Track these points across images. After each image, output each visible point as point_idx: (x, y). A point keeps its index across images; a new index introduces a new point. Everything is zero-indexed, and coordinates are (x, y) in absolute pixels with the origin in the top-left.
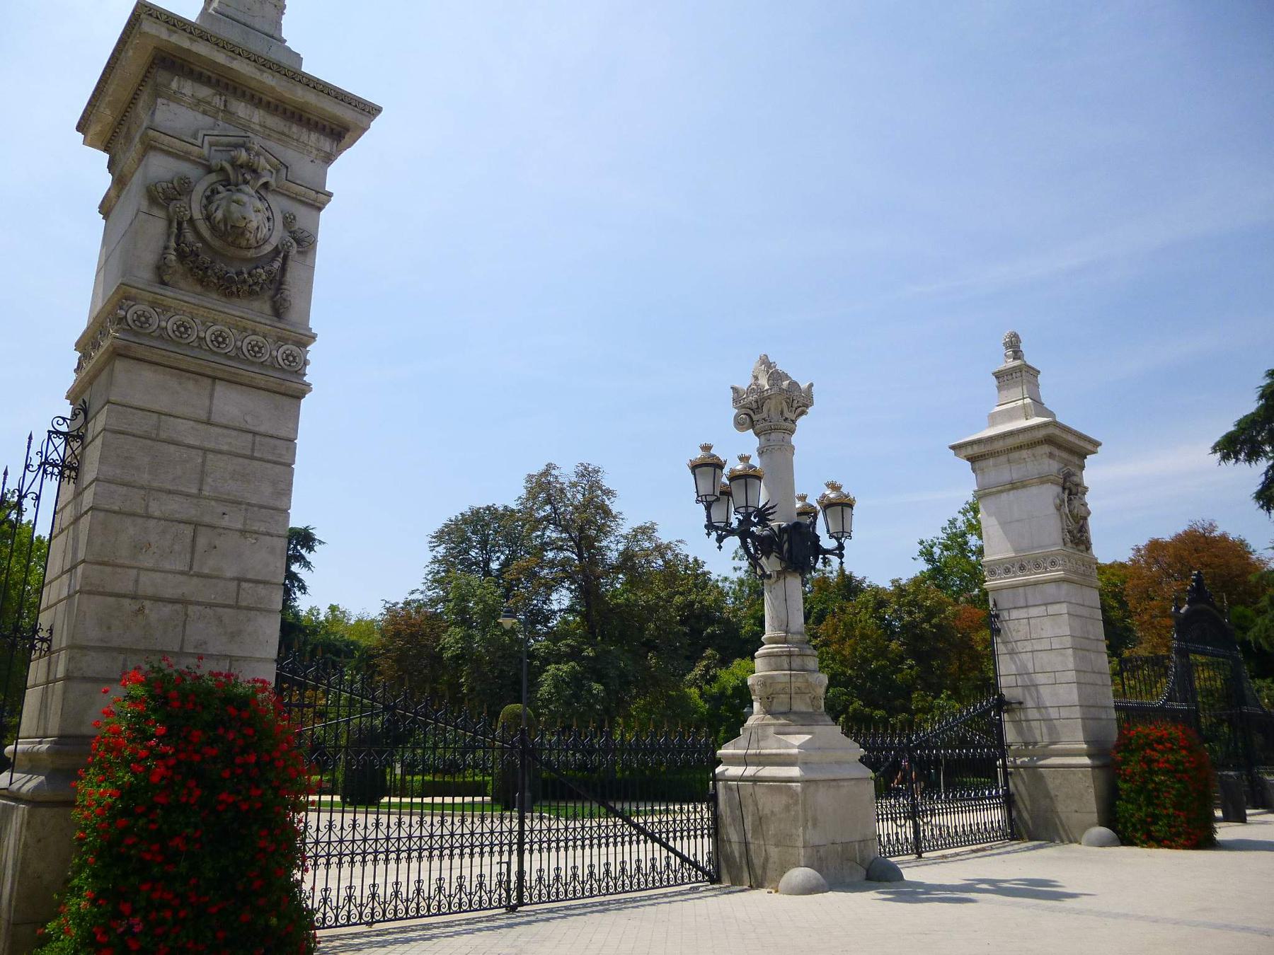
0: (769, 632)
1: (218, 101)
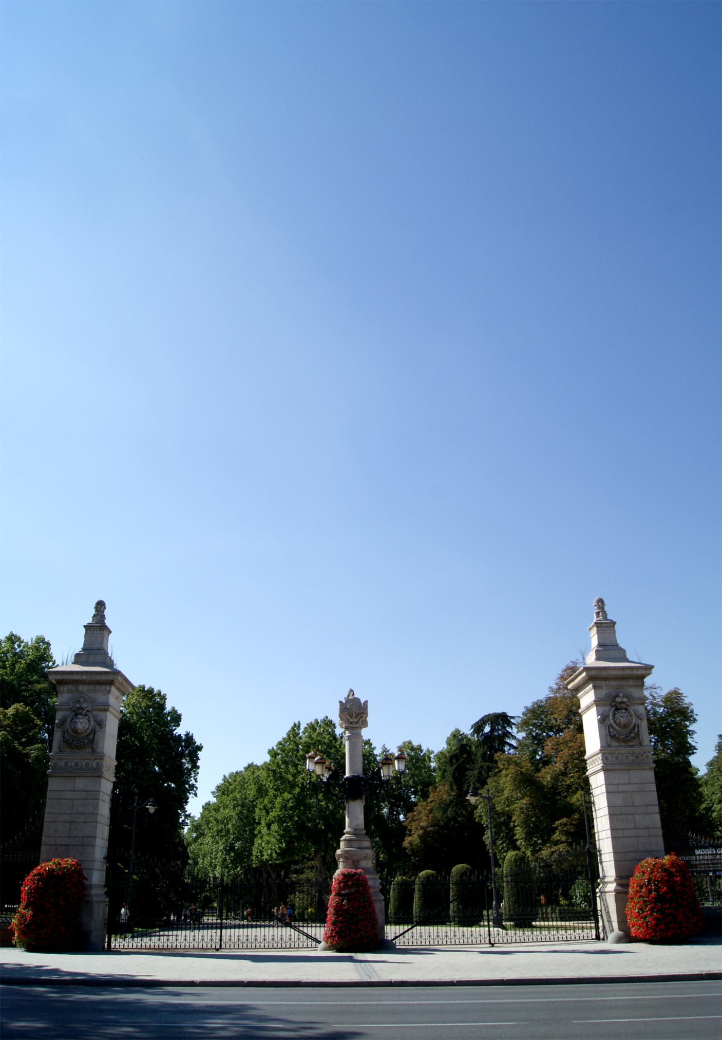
0: (347, 829)
1: (74, 688)
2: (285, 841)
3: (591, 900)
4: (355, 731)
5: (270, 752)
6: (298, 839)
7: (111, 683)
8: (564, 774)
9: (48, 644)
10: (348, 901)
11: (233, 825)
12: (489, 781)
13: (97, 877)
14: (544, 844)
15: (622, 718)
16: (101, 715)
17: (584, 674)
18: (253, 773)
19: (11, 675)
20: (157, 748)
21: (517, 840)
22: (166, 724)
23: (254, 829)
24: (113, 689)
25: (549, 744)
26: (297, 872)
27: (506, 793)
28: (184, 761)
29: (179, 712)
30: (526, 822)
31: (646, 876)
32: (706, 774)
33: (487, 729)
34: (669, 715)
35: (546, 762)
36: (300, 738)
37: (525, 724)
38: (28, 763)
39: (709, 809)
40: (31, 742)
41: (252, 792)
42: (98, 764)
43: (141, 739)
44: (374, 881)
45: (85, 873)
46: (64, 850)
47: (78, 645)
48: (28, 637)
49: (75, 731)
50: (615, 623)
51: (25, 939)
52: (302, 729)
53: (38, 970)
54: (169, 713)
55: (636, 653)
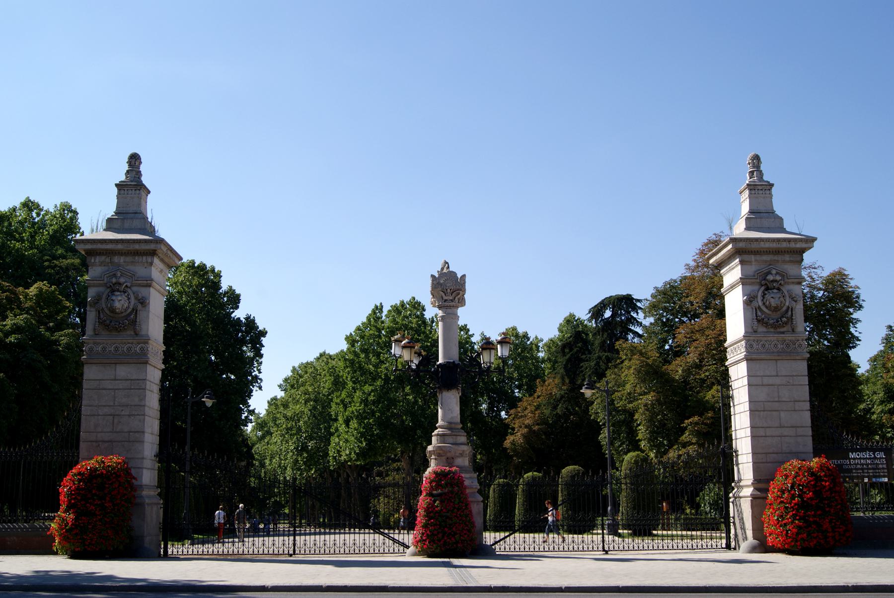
0: (440, 422)
1: (108, 260)
2: (365, 440)
3: (722, 506)
4: (449, 311)
5: (347, 338)
6: (381, 438)
7: (153, 253)
8: (699, 366)
9: (75, 213)
10: (441, 502)
11: (305, 423)
12: (608, 373)
13: (148, 476)
14: (671, 446)
15: (773, 299)
16: (143, 291)
17: (730, 246)
18: (327, 363)
19: (31, 248)
20: (212, 334)
21: (640, 440)
22: (222, 306)
23: (330, 427)
24: (156, 261)
25: (682, 331)
26: (380, 474)
27: (628, 388)
28: (245, 348)
29: (237, 292)
30: (651, 420)
31: (790, 480)
32: (868, 371)
33: (608, 314)
34: (830, 300)
35: (678, 352)
36: (383, 322)
37: (653, 308)
38: (58, 351)
39: (868, 411)
40: (59, 327)
41: (326, 384)
42: (142, 349)
43: (192, 324)
44: (471, 481)
45: (133, 472)
46: (109, 447)
47: (109, 207)
48: (49, 203)
49: (113, 310)
50: (772, 185)
51: (67, 545)
52: (385, 312)
53: (90, 576)
54: (226, 293)
55: (795, 219)
